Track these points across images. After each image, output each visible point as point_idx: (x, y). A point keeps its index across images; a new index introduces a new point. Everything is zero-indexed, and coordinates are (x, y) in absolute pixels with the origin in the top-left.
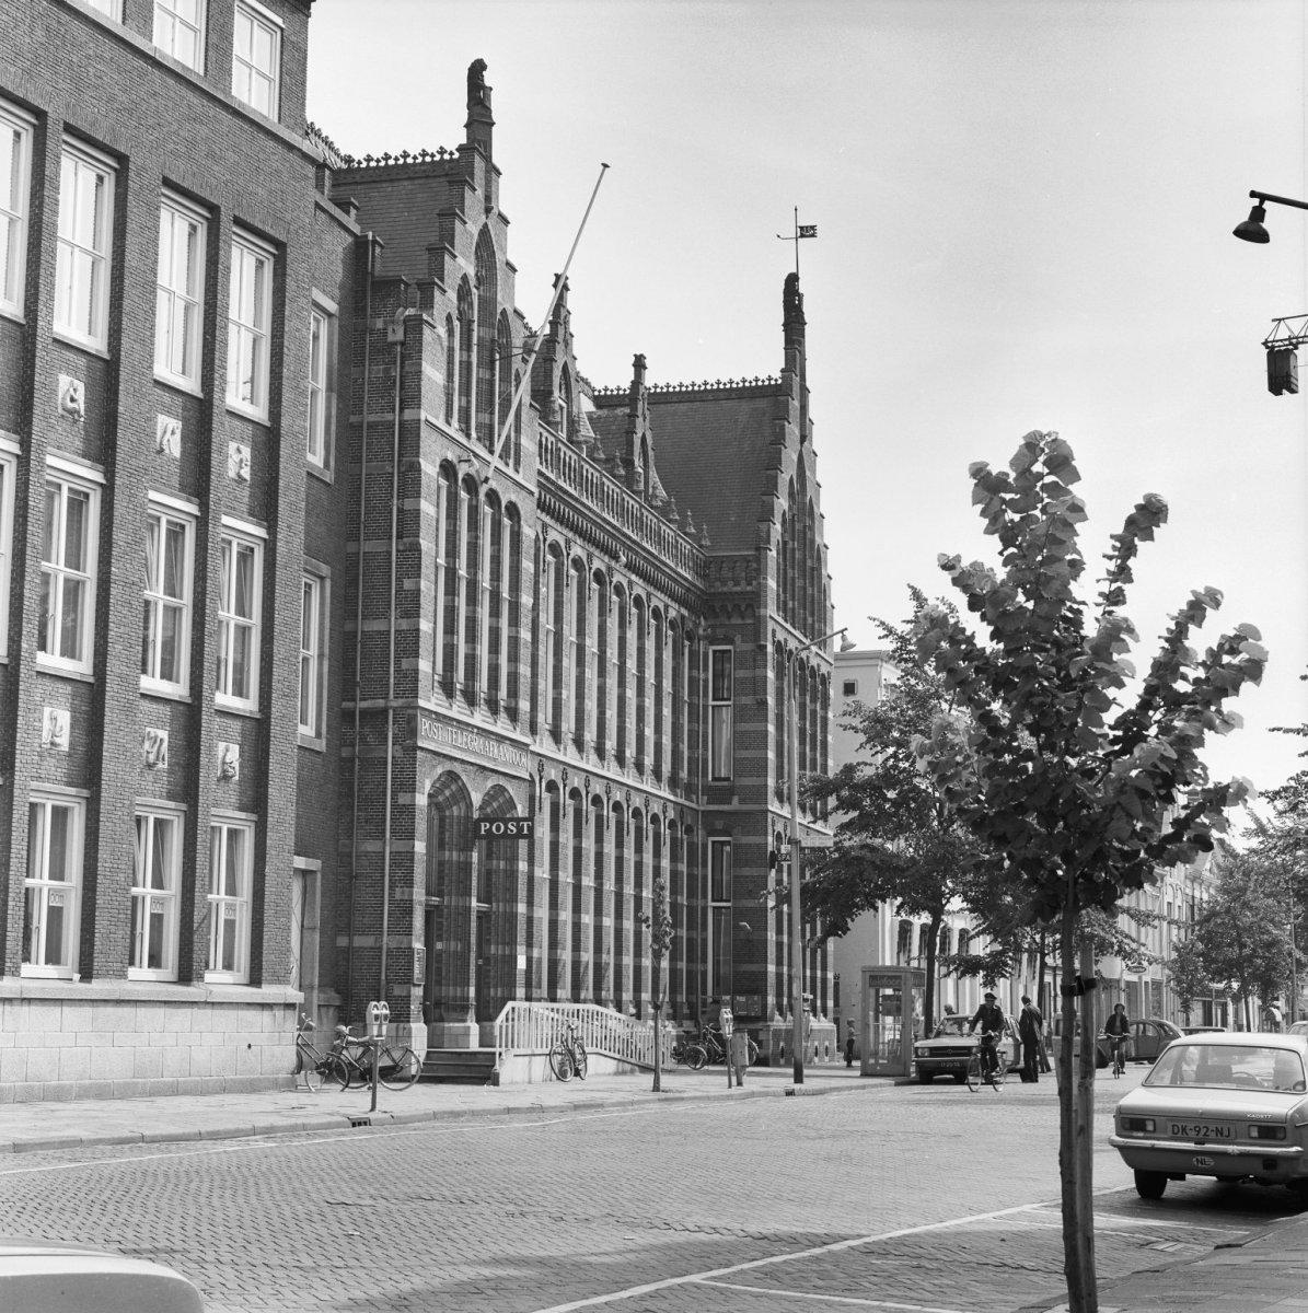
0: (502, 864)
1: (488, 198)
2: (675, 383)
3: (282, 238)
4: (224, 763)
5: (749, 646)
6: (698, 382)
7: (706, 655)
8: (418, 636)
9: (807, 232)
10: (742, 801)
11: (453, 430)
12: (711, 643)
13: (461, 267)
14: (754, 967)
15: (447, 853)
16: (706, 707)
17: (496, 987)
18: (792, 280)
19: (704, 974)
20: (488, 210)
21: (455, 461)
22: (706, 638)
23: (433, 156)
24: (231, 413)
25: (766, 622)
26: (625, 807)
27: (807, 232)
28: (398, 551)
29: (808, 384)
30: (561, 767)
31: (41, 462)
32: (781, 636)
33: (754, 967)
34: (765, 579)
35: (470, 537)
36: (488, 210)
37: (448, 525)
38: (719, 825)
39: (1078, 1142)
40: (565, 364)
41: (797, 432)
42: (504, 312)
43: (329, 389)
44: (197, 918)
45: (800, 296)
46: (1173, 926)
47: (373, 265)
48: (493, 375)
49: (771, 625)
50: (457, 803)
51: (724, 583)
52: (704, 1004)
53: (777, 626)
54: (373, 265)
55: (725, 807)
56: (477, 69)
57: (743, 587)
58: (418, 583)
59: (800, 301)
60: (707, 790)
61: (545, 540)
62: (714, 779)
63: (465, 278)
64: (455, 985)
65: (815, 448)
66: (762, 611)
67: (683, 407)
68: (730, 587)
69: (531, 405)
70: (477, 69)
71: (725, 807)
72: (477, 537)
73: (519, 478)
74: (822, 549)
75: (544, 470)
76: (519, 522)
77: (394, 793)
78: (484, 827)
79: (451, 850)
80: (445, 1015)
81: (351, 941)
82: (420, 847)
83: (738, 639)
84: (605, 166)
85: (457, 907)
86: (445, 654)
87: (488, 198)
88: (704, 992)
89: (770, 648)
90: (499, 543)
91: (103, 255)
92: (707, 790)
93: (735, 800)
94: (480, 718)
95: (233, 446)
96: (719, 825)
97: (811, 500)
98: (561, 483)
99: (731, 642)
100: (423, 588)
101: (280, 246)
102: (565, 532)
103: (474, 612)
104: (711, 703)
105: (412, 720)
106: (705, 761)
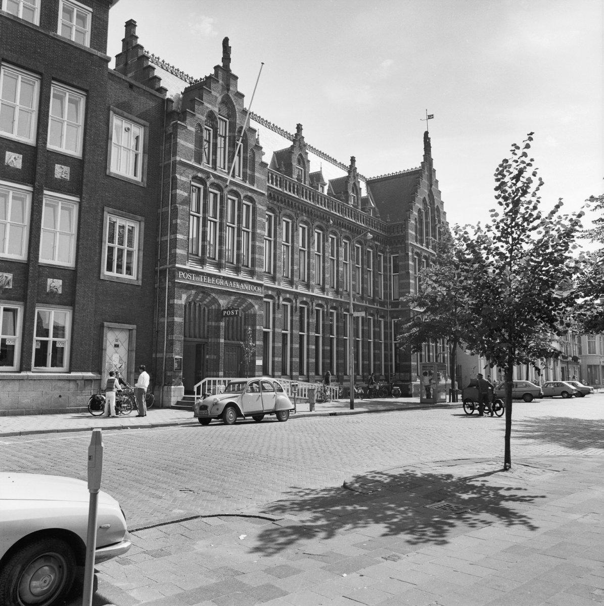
2: (391, 173)
3: (88, 88)
7: (390, 258)
8: (176, 241)
9: (431, 117)
10: (402, 307)
12: (392, 254)
13: (207, 108)
14: (407, 363)
16: (390, 276)
18: (426, 134)
19: (391, 366)
22: (390, 252)
27: (431, 117)
28: (171, 210)
33: (407, 363)
37: (203, 201)
39: (59, 356)
43: (144, 152)
45: (429, 139)
46: (231, 261)
50: (213, 304)
51: (394, 233)
52: (392, 376)
55: (397, 309)
56: (226, 41)
57: (401, 234)
58: (177, 221)
60: (391, 303)
62: (394, 300)
65: (440, 189)
66: (407, 241)
67: (393, 180)
68: (397, 234)
70: (226, 41)
71: (397, 309)
73: (255, 188)
76: (255, 204)
77: (168, 300)
78: (225, 312)
84: (263, 63)
86: (202, 249)
88: (392, 371)
91: (34, 109)
92: (391, 303)
93: (400, 306)
94: (210, 269)
99: (398, 253)
104: (392, 274)
105: (174, 272)
106: (390, 294)
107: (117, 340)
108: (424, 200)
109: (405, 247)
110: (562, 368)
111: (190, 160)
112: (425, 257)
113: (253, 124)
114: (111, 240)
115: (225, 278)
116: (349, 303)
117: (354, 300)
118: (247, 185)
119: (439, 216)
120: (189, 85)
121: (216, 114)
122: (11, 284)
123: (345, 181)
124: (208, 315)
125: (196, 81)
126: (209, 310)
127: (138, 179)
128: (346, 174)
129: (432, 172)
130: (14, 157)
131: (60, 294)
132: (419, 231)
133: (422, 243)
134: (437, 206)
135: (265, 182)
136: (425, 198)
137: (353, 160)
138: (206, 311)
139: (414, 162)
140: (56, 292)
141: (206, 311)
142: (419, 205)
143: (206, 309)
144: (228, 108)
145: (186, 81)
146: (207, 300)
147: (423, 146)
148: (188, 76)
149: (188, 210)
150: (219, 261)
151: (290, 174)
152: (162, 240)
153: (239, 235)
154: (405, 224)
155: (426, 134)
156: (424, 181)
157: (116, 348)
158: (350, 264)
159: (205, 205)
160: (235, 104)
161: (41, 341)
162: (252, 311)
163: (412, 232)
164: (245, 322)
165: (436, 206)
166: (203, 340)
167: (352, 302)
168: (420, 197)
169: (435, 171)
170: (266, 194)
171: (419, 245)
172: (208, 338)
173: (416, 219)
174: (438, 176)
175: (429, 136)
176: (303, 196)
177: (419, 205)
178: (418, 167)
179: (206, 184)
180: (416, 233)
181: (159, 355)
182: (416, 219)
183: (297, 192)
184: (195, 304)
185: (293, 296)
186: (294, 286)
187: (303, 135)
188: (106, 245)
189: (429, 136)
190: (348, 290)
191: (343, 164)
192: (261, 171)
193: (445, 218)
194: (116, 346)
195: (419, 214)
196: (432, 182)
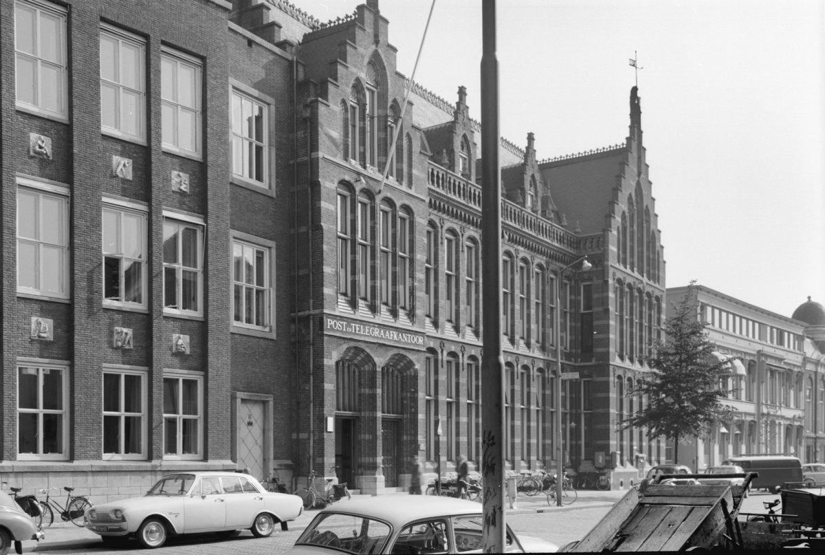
0: (409, 394)
1: (376, 36)
4: (177, 345)
5: (600, 281)
6: (333, 19)
11: (404, 188)
13: (352, 73)
15: (362, 390)
17: (407, 456)
18: (634, 90)
20: (377, 42)
21: (352, 181)
23: (351, 17)
24: (165, 153)
25: (608, 268)
26: (439, 351)
29: (645, 144)
30: (461, 345)
31: (13, 182)
32: (619, 275)
34: (608, 246)
35: (410, 237)
36: (377, 42)
38: (586, 372)
40: (465, 136)
41: (636, 170)
42: (653, 231)
43: (270, 145)
44: (154, 424)
45: (638, 99)
47: (297, 75)
48: (387, 135)
49: (611, 271)
53: (617, 269)
54: (297, 75)
55: (588, 364)
59: (638, 102)
61: (517, 257)
63: (624, 213)
64: (369, 456)
66: (606, 263)
69: (421, 153)
71: (588, 364)
72: (375, 223)
73: (412, 192)
74: (656, 233)
75: (432, 187)
79: (364, 388)
80: (363, 472)
81: (298, 435)
82: (379, 391)
83: (595, 278)
85: (369, 417)
87: (376, 36)
89: (611, 281)
90: (396, 227)
95: (175, 173)
96: (586, 372)
97: (647, 206)
98: (540, 237)
100: (397, 270)
101: (203, 58)
102: (460, 223)
103: (355, 257)
107: (250, 417)
108: (630, 197)
109: (603, 270)
110: (808, 447)
111: (335, 156)
112: (629, 286)
113: (412, 97)
114: (238, 278)
115: (381, 326)
116: (557, 362)
117: (562, 359)
118: (404, 188)
119: (648, 222)
120: (311, 31)
121: (363, 83)
122: (131, 343)
123: (449, 129)
124: (360, 379)
125: (322, 25)
126: (360, 372)
127: (263, 186)
128: (450, 118)
129: (641, 150)
130: (123, 163)
131: (188, 355)
132: (622, 246)
133: (625, 264)
134: (647, 206)
135: (425, 183)
136: (630, 195)
137: (531, 138)
138: (357, 374)
139: (618, 136)
140: (184, 352)
141: (357, 374)
142: (623, 206)
143: (357, 371)
144: (376, 71)
145: (298, 20)
146: (359, 358)
147: (628, 110)
148: (287, 3)
149: (334, 231)
150: (372, 303)
151: (452, 166)
152: (300, 274)
153: (373, 257)
154: (604, 237)
155: (634, 90)
156: (632, 169)
157: (250, 427)
158: (556, 308)
159: (457, 261)
160: (385, 64)
161: (55, 407)
162: (410, 372)
163: (613, 248)
164: (402, 387)
165: (645, 205)
166: (356, 414)
167: (560, 361)
168: (623, 197)
169: (645, 149)
170: (427, 200)
171: (622, 267)
172: (360, 411)
173: (618, 227)
174: (649, 158)
175: (639, 95)
176: (450, 193)
177: (623, 206)
178: (619, 143)
179: (355, 191)
180: (619, 249)
181: (303, 436)
182: (618, 227)
183: (464, 195)
184: (343, 364)
185: (459, 348)
186: (440, 330)
187: (535, 148)
188: (233, 282)
189: (639, 94)
190: (555, 344)
191: (506, 140)
192: (420, 168)
193: (656, 225)
194: (250, 424)
195: (622, 219)
196: (642, 168)
